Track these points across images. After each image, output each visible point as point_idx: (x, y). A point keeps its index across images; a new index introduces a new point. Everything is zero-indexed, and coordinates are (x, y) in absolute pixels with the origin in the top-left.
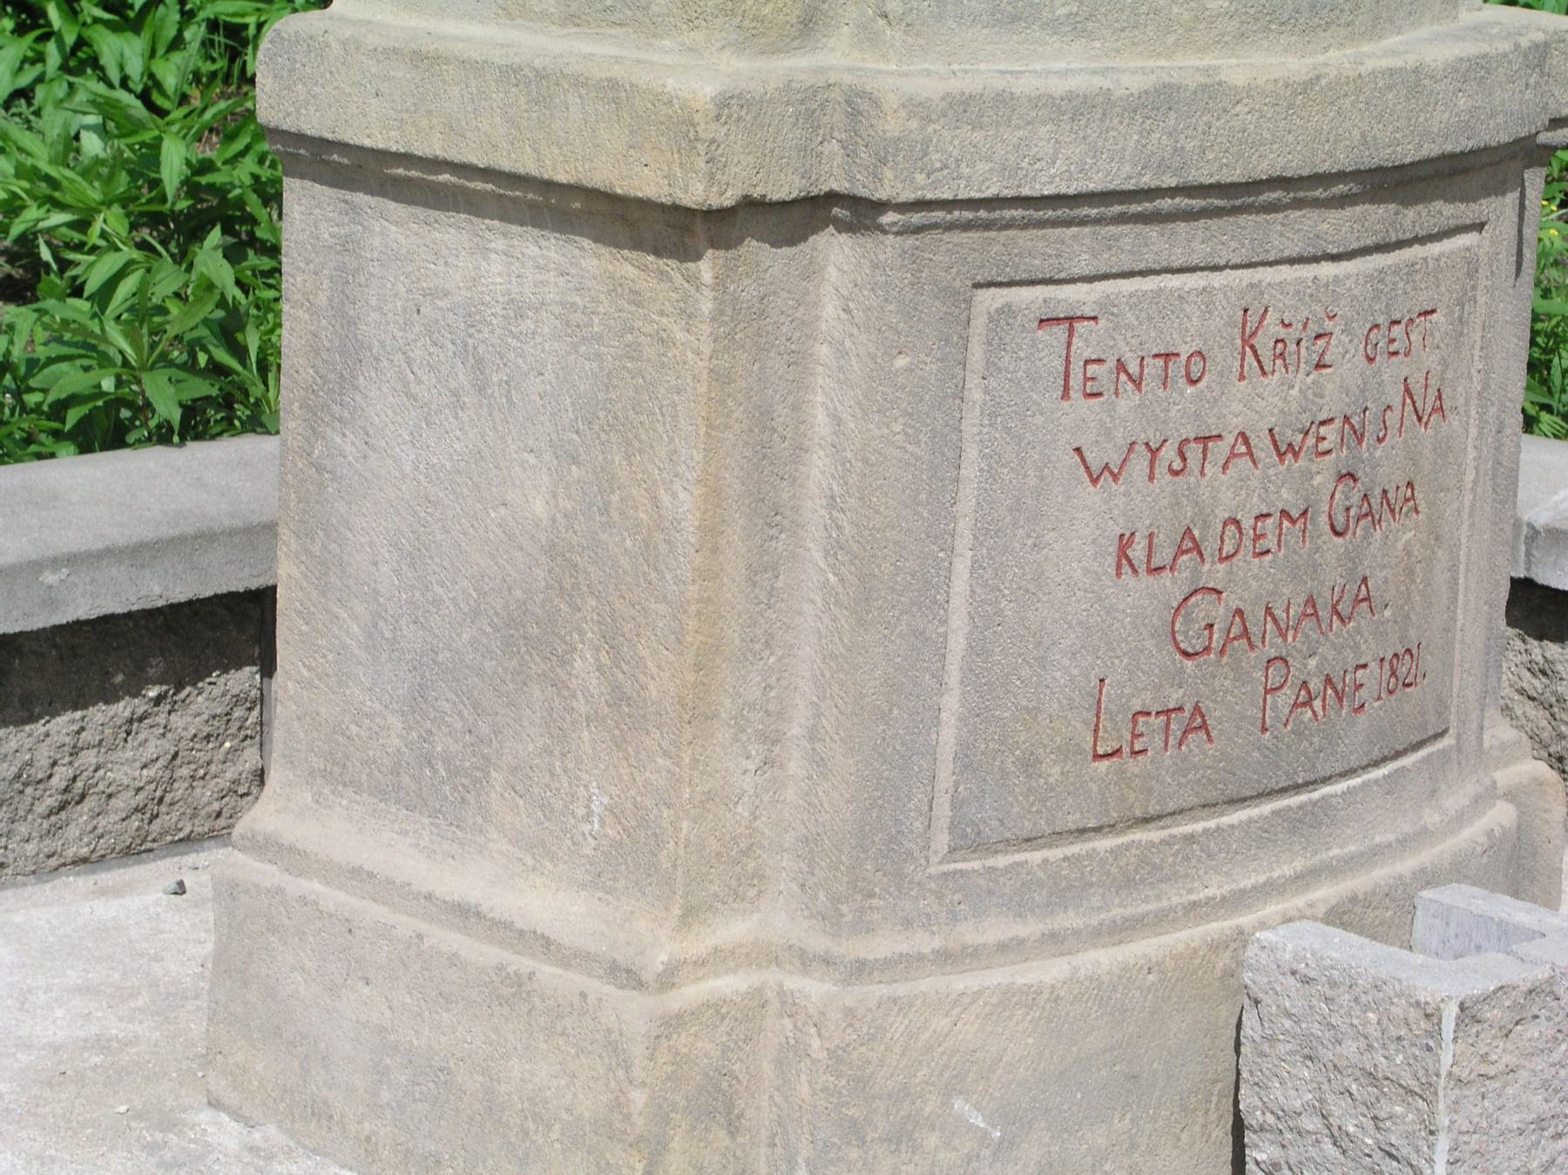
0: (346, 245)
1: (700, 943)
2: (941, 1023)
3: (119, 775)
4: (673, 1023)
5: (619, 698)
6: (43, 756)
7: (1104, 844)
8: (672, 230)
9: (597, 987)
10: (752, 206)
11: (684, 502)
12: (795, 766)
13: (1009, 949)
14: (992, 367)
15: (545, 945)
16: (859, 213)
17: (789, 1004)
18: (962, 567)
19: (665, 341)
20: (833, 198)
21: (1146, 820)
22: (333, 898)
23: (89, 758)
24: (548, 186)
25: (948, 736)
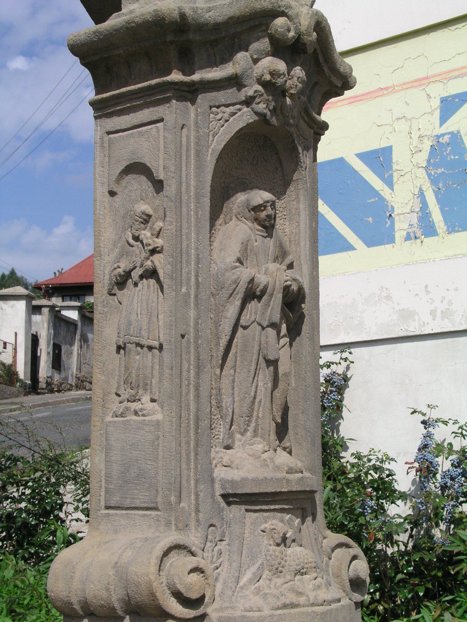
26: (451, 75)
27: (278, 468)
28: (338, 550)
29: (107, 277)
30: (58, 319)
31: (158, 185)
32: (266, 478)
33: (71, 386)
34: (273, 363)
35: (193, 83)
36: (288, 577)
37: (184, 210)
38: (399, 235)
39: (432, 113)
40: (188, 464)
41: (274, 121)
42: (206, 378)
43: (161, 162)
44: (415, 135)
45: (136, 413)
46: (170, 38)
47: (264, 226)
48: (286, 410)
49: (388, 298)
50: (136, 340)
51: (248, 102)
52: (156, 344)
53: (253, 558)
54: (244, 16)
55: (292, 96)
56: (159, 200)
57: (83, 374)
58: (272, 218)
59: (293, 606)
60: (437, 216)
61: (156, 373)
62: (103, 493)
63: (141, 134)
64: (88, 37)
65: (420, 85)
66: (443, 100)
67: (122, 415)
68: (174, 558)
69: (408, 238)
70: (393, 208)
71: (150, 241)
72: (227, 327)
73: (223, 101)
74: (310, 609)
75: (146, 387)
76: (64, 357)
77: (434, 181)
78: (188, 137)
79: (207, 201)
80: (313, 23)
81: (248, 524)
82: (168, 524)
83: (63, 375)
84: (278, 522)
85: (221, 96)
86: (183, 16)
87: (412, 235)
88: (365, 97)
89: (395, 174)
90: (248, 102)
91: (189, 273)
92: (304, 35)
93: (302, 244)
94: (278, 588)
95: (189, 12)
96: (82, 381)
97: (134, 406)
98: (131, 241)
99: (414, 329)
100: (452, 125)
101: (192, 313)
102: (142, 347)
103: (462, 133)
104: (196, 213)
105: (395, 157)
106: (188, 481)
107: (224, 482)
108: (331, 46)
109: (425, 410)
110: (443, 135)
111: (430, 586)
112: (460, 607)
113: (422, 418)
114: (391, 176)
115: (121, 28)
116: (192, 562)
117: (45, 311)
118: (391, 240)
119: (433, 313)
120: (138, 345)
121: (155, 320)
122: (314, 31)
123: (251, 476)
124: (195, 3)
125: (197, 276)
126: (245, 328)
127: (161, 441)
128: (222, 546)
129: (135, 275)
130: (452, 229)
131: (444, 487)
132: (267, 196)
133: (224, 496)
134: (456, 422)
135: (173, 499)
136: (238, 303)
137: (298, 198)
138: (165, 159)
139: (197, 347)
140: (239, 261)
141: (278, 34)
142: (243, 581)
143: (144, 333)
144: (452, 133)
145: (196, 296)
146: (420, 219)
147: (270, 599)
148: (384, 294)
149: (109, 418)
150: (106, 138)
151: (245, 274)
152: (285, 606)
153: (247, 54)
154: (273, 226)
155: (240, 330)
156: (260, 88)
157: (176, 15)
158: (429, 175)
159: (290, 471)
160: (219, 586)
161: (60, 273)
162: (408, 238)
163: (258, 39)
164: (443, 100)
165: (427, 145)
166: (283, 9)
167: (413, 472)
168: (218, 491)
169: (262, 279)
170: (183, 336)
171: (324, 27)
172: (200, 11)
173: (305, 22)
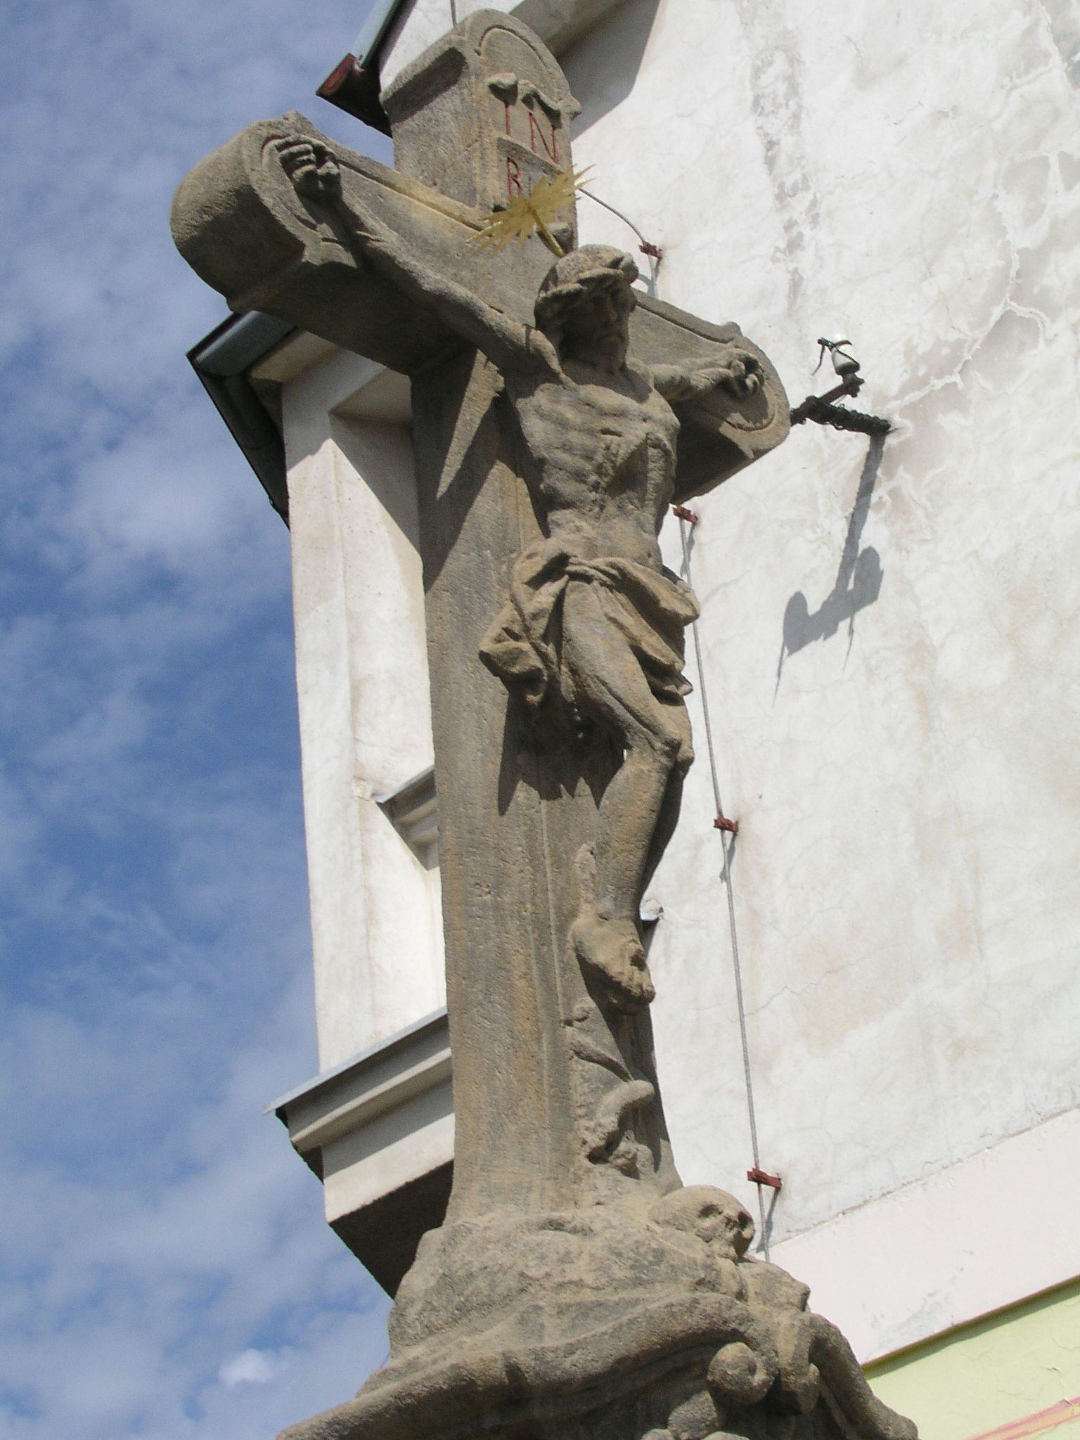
46: (491, 1421)
54: (649, 1353)
64: (318, 1434)
80: (806, 1346)
86: (513, 1371)
88: (1028, 1427)
92: (788, 1374)
95: (526, 1362)
108: (857, 1386)
115: (386, 1409)
122: (811, 1360)
124: (541, 1337)
141: (729, 1383)
153: (666, 1432)
157: (498, 1371)
163: (686, 1397)
166: (733, 1325)
171: (834, 1348)
172: (550, 1356)
173: (788, 1345)
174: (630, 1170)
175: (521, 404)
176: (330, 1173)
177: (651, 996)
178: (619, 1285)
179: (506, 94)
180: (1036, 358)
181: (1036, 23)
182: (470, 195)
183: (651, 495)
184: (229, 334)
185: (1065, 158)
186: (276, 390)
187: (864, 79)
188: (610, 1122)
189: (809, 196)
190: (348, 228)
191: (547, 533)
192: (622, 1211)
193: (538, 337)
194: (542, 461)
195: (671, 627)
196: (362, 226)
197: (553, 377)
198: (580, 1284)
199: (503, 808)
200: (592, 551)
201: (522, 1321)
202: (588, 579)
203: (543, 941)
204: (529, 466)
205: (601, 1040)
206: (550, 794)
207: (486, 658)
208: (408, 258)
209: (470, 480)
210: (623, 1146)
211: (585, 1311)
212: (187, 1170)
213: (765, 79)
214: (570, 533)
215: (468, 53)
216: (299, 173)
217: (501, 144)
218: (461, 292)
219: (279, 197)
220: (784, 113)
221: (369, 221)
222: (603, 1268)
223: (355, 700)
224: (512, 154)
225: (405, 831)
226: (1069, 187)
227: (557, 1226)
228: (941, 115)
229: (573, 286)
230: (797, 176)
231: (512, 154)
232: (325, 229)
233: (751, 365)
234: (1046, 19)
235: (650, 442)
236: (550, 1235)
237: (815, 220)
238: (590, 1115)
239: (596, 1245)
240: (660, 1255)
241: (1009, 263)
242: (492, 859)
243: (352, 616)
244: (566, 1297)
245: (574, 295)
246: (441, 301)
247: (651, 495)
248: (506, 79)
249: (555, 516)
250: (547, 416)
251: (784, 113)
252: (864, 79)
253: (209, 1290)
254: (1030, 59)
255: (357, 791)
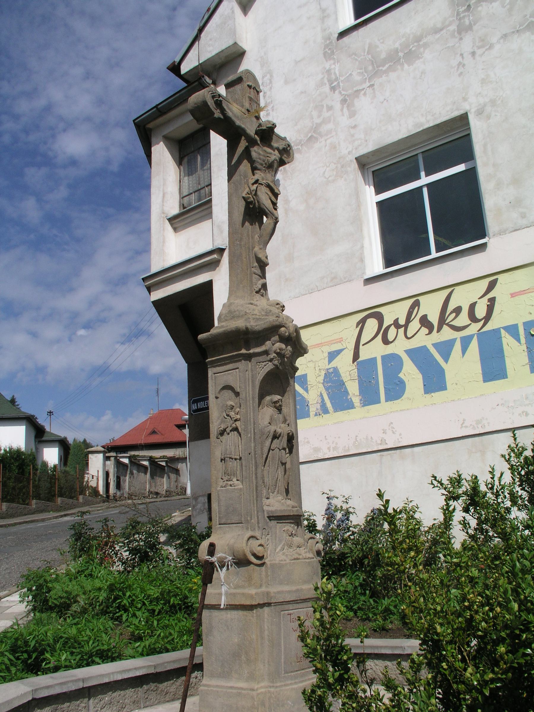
0: (210, 616)
1: (259, 686)
2: (286, 692)
3: (171, 690)
4: (258, 694)
5: (248, 660)
6: (164, 688)
7: (299, 672)
8: (250, 608)
9: (249, 692)
10: (259, 604)
11: (254, 636)
12: (267, 666)
13: (291, 684)
14: (283, 620)
15: (242, 689)
16: (269, 604)
17: (269, 692)
18: (282, 641)
19: (250, 620)
20: (266, 603)
21: (303, 669)
22: (215, 689)
23: (168, 688)
24: (236, 605)
25: (283, 660)
26: (332, 342)
27: (288, 506)
28: (310, 540)
29: (216, 431)
30: (119, 464)
31: (237, 394)
32: (284, 510)
33: (126, 498)
34: (284, 464)
35: (250, 354)
36: (295, 548)
37: (248, 403)
38: (312, 414)
39: (324, 359)
40: (254, 505)
41: (280, 367)
42: (259, 471)
43: (238, 385)
44: (317, 369)
45: (231, 485)
47: (278, 409)
48: (288, 483)
49: (308, 442)
50: (229, 456)
51: (271, 360)
52: (238, 457)
53: (281, 541)
55: (287, 358)
56: (237, 400)
57: (131, 491)
58: (281, 406)
59: (297, 559)
60: (329, 405)
61: (238, 469)
62: (218, 519)
63: (229, 374)
65: (318, 347)
66: (329, 353)
67: (224, 487)
68: (251, 541)
69: (316, 415)
70: (308, 401)
71: (234, 416)
72: (266, 450)
73: (261, 360)
74: (304, 560)
75: (235, 475)
76: (122, 483)
77: (327, 389)
78: (248, 375)
79: (257, 400)
81: (278, 528)
82: (247, 529)
83: (122, 492)
84: (290, 527)
85: (261, 358)
86: (247, 328)
87: (318, 414)
89: (309, 386)
90: (271, 360)
91: (251, 429)
93: (292, 416)
94: (292, 552)
95: (249, 327)
96: (131, 495)
97: (229, 483)
98: (226, 417)
99: (321, 456)
100: (334, 364)
101: (253, 445)
102: (232, 459)
103: (338, 368)
104: (253, 405)
105: (309, 378)
106: (254, 512)
107: (268, 512)
109: (328, 492)
110: (330, 369)
111: (334, 569)
112: (348, 576)
113: (327, 496)
114: (307, 387)
116: (259, 542)
117: (112, 459)
118: (308, 416)
119: (329, 448)
120: (230, 458)
121: (237, 448)
123: (278, 509)
125: (254, 430)
126: (273, 450)
127: (242, 496)
128: (268, 537)
129: (228, 430)
130: (336, 410)
131: (339, 526)
132: (279, 397)
133: (268, 517)
134: (344, 496)
135: (249, 518)
136: (270, 440)
137: (289, 398)
138: (240, 384)
139: (255, 458)
140: (270, 423)
142: (278, 550)
143: (233, 453)
144: (334, 368)
145: (254, 438)
146: (321, 406)
147: (289, 557)
148: (306, 441)
149: (219, 488)
150: (214, 376)
151: (272, 428)
152: (295, 559)
154: (281, 409)
155: (271, 451)
156: (275, 355)
157: (244, 328)
158: (324, 386)
159: (293, 507)
160: (269, 552)
161: (113, 440)
162: (316, 415)
164: (329, 353)
165: (323, 373)
167: (325, 519)
168: (266, 515)
169: (279, 431)
170: (250, 454)
173: (292, 329)
174: (262, 295)
175: (251, 149)
176: (153, 291)
177: (268, 264)
178: (263, 315)
179: (250, 87)
180: (317, 145)
181: (324, 77)
182: (242, 106)
183: (274, 170)
184: (144, 116)
185: (327, 105)
186: (151, 130)
187: (286, 82)
188: (260, 286)
189: (272, 105)
190: (223, 111)
191: (254, 175)
192: (262, 303)
193: (256, 136)
194: (255, 161)
195: (276, 195)
196: (226, 111)
197: (258, 145)
198: (256, 314)
199: (242, 226)
200: (263, 179)
201: (246, 320)
202: (262, 185)
203: (249, 252)
204: (252, 161)
205: (258, 271)
206: (252, 225)
207: (243, 198)
208: (234, 118)
209: (239, 162)
210: (262, 291)
211: (258, 319)
212: (71, 290)
213: (265, 79)
214: (259, 175)
215: (243, 78)
216: (215, 99)
217: (249, 97)
218: (243, 126)
219: (211, 103)
220: (268, 87)
221: (227, 110)
222: (260, 312)
223: (164, 196)
224: (251, 99)
225: (172, 225)
226: (327, 112)
227: (252, 304)
228: (302, 93)
229: (265, 128)
230: (270, 100)
231: (251, 99)
232: (219, 111)
233: (289, 146)
234: (326, 76)
235: (276, 160)
236: (250, 305)
237: (273, 110)
238: (256, 285)
239: (259, 308)
240: (271, 311)
241: (313, 125)
242: (240, 236)
243: (164, 179)
244: (254, 316)
245: (265, 130)
246: (239, 127)
247: (274, 170)
248: (250, 84)
249: (255, 172)
250: (256, 152)
251: (268, 87)
252: (286, 82)
253: (75, 315)
254: (322, 84)
255: (163, 216)
